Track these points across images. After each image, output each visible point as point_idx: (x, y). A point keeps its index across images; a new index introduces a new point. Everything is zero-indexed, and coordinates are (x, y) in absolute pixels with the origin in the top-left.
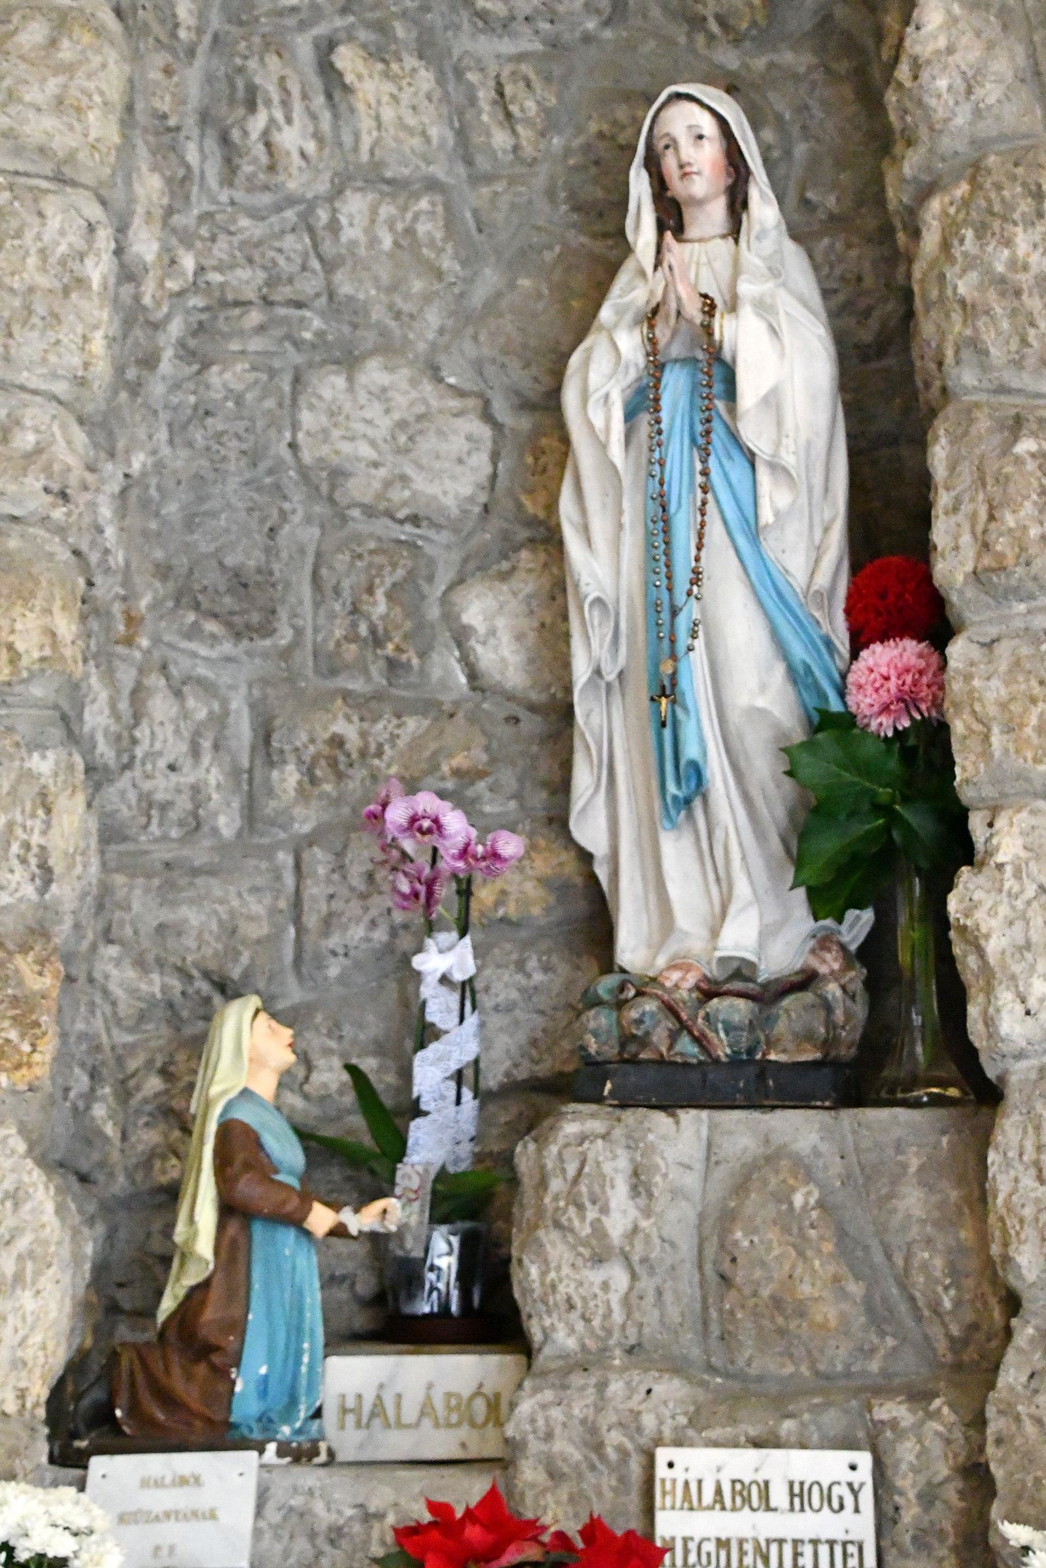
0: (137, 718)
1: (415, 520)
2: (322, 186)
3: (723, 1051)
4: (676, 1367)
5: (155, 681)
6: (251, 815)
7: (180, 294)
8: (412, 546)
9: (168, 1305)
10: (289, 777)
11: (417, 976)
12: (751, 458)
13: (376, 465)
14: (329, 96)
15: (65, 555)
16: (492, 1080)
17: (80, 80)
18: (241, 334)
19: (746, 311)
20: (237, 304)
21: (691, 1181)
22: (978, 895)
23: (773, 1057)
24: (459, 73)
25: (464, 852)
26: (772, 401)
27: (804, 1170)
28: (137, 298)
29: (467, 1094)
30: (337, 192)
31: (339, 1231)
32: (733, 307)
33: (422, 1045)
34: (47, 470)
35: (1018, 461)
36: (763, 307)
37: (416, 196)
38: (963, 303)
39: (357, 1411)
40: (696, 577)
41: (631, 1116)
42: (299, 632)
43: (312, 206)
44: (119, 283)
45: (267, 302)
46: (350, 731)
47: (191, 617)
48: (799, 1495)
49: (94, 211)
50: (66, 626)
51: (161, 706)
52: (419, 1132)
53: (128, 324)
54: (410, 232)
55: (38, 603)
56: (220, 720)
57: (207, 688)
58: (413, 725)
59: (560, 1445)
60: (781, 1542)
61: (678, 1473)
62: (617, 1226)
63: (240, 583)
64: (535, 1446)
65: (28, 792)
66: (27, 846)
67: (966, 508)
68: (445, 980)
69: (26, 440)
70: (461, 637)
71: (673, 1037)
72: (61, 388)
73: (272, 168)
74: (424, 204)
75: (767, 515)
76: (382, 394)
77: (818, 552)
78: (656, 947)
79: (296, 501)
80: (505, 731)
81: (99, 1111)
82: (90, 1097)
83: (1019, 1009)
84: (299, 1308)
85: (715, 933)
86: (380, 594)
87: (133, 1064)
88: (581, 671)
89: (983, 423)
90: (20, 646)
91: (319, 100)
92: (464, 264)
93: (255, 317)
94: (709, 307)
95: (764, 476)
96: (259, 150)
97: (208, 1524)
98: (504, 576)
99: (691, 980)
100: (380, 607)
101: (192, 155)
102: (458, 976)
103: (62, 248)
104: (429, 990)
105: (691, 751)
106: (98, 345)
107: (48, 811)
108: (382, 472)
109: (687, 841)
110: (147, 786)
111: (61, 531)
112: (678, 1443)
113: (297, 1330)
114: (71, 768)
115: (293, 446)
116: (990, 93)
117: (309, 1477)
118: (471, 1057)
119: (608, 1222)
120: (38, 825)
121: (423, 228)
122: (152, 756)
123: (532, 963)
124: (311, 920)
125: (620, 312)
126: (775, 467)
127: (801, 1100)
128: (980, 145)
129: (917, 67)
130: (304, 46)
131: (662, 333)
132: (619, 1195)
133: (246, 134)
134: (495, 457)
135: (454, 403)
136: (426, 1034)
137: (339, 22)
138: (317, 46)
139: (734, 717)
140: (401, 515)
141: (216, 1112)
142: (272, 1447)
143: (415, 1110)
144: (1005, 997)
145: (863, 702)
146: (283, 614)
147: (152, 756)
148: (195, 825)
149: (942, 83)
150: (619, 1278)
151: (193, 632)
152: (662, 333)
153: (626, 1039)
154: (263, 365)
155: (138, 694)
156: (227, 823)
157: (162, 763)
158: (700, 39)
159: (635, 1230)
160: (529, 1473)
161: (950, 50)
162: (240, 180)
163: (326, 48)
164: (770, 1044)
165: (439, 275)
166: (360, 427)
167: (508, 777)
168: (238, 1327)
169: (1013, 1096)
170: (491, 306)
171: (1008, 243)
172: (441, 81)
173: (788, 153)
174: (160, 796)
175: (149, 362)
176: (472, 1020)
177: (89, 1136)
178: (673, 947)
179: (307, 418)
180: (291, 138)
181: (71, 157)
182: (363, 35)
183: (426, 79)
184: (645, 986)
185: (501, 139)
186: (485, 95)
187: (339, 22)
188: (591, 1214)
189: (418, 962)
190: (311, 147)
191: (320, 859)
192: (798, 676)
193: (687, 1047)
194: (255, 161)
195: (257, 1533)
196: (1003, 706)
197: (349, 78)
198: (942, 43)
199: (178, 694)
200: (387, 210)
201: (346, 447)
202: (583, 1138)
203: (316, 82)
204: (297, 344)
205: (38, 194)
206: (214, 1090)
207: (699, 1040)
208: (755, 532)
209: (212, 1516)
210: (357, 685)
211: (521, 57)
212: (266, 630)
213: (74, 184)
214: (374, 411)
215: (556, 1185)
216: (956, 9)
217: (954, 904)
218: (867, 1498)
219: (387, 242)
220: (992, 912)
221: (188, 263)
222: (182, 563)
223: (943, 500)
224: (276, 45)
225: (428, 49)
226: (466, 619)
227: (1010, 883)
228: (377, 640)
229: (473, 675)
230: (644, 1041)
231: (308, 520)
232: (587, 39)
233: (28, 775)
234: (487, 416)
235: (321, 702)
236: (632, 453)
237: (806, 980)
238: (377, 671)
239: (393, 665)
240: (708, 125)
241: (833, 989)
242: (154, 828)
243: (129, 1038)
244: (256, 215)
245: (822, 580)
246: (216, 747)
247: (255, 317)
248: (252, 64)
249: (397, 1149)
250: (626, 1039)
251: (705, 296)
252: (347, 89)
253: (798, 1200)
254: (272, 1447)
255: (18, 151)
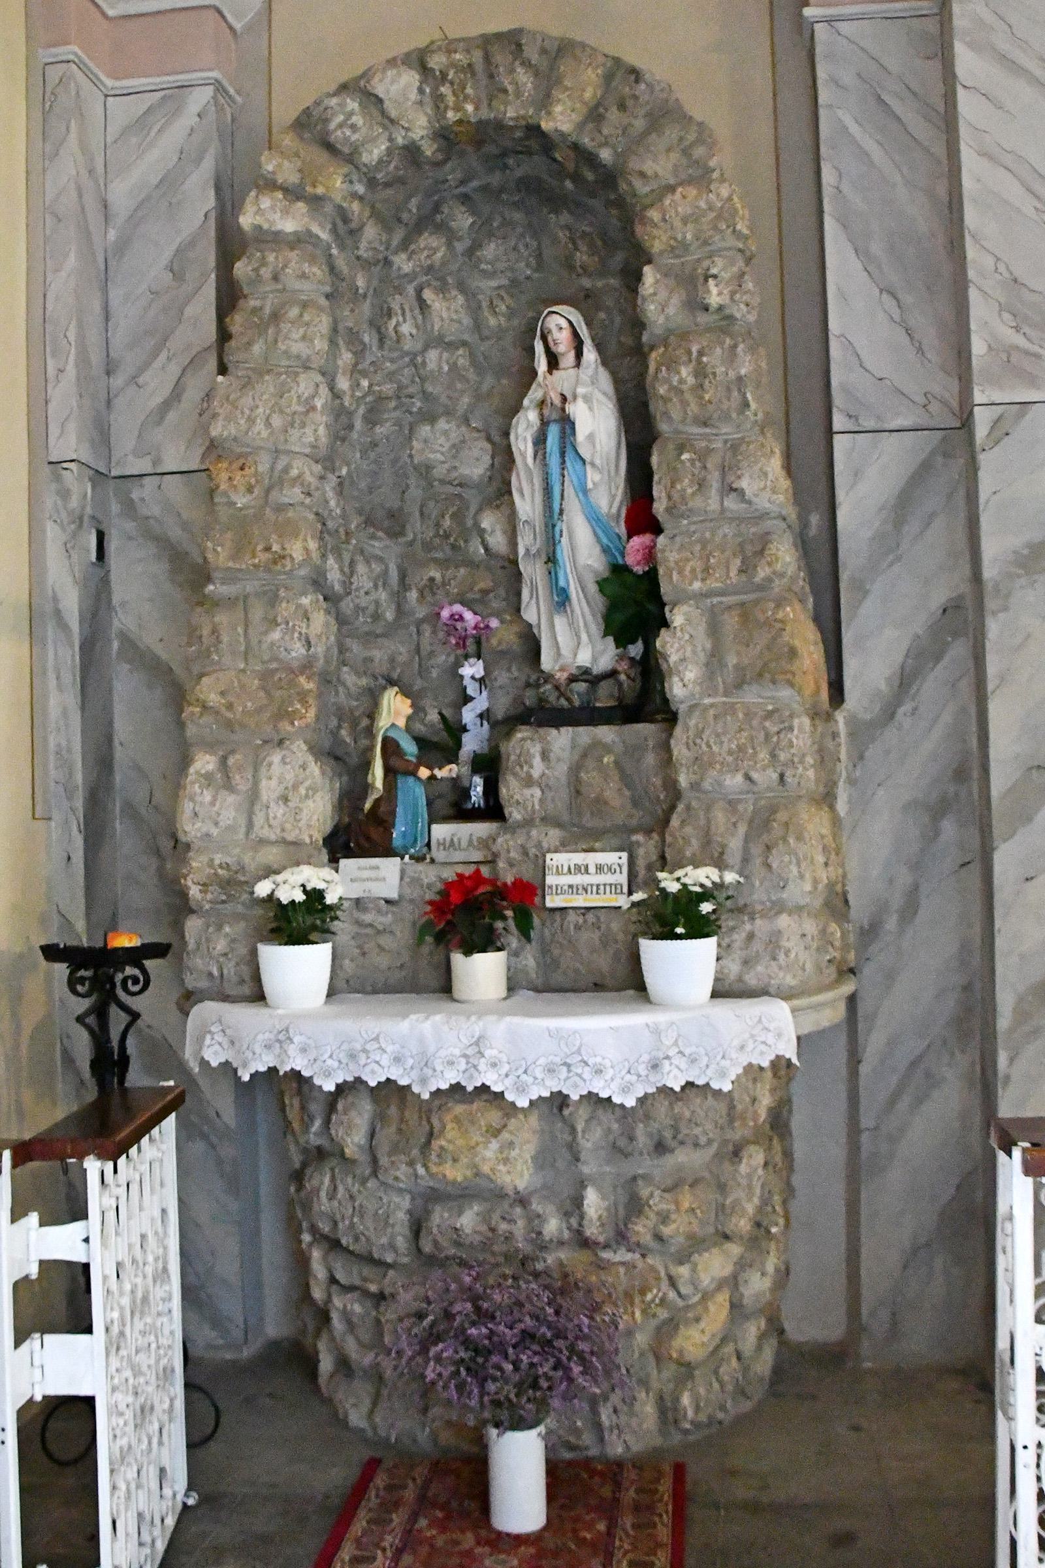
0: (352, 573)
1: (460, 485)
2: (419, 346)
3: (577, 703)
4: (559, 825)
5: (359, 558)
6: (400, 611)
7: (364, 397)
8: (459, 496)
9: (368, 806)
10: (413, 595)
11: (462, 677)
12: (584, 461)
13: (443, 462)
14: (421, 309)
15: (311, 517)
16: (500, 715)
17: (312, 329)
18: (389, 411)
19: (580, 402)
20: (387, 398)
21: (566, 755)
22: (668, 639)
23: (598, 705)
24: (474, 295)
25: (476, 627)
26: (591, 437)
27: (607, 749)
28: (342, 404)
29: (485, 723)
30: (426, 347)
31: (432, 777)
32: (575, 397)
33: (465, 704)
34: (302, 484)
35: (682, 462)
36: (587, 399)
37: (457, 348)
38: (662, 397)
39: (444, 844)
40: (561, 512)
41: (542, 731)
42: (415, 535)
43: (415, 355)
44: (333, 400)
45: (399, 398)
46: (437, 575)
47: (372, 530)
48: (600, 868)
49: (319, 378)
50: (313, 545)
51: (361, 568)
52: (466, 738)
53: (337, 416)
54: (455, 364)
55: (301, 537)
56: (386, 572)
57: (380, 559)
58: (462, 571)
59: (513, 854)
60: (592, 885)
61: (554, 863)
62: (536, 773)
63: (391, 515)
64: (503, 855)
65: (300, 612)
66: (300, 633)
67: (663, 481)
68: (473, 677)
69: (294, 472)
70: (481, 532)
71: (558, 698)
72: (307, 451)
73: (398, 341)
74: (461, 352)
75: (590, 485)
76: (446, 433)
77: (613, 497)
78: (556, 661)
79: (412, 481)
80: (499, 572)
81: (343, 732)
82: (339, 727)
83: (681, 684)
84: (416, 806)
85: (575, 655)
86: (447, 517)
87: (357, 714)
88: (521, 551)
89: (671, 446)
90: (295, 556)
91: (417, 311)
92: (479, 374)
93: (393, 404)
94: (564, 399)
95: (588, 467)
96: (393, 334)
97: (382, 883)
98: (498, 507)
99: (565, 675)
100: (447, 522)
101: (366, 339)
102: (478, 676)
103: (306, 395)
104: (467, 682)
105: (562, 583)
106: (322, 430)
107: (308, 619)
108: (446, 466)
109: (565, 620)
110: (357, 601)
111: (309, 507)
112: (556, 852)
113: (415, 815)
114: (318, 600)
115: (411, 456)
116: (671, 310)
117: (420, 867)
118: (485, 708)
119: (532, 771)
120: (304, 625)
121: (461, 361)
122: (357, 590)
123: (514, 669)
124: (424, 653)
125: (531, 402)
126: (593, 464)
127: (608, 721)
128: (670, 332)
129: (644, 299)
130: (411, 290)
131: (546, 412)
132: (537, 761)
133: (387, 329)
134: (493, 457)
135: (476, 435)
136: (467, 699)
137: (425, 278)
138: (416, 290)
139: (580, 568)
140: (456, 483)
141: (382, 732)
142: (407, 857)
143: (464, 729)
144: (676, 679)
145: (630, 560)
146: (408, 527)
147: (357, 590)
148: (376, 617)
149: (652, 307)
150: (537, 793)
151: (373, 537)
152: (546, 412)
153: (541, 700)
154: (398, 423)
155: (352, 563)
156: (390, 615)
157: (362, 592)
158: (574, 276)
159: (544, 774)
160: (501, 864)
161: (655, 294)
162: (386, 347)
163: (419, 291)
164: (596, 700)
165: (468, 381)
166: (437, 447)
167: (502, 592)
168: (393, 813)
169: (680, 717)
170: (489, 394)
171: (679, 373)
172: (467, 300)
173: (612, 322)
174: (363, 605)
175: (350, 427)
176: (485, 693)
177: (340, 742)
178: (561, 662)
179: (415, 443)
180: (406, 329)
181: (308, 359)
182: (434, 283)
183: (461, 299)
184: (548, 678)
185: (493, 322)
186: (485, 304)
187: (425, 278)
188: (525, 768)
189: (462, 671)
190: (414, 332)
191: (427, 630)
192: (605, 550)
193: (563, 702)
194: (391, 339)
195: (401, 885)
196: (676, 563)
197: (429, 302)
198: (651, 291)
199: (368, 562)
200: (445, 355)
201: (432, 456)
202: (523, 739)
203: (416, 304)
204: (411, 413)
205: (297, 374)
206: (381, 724)
207: (568, 699)
208: (585, 492)
209: (384, 879)
210: (439, 555)
211: (499, 287)
212: (402, 533)
213: (310, 368)
214: (442, 440)
215: (513, 758)
216: (658, 276)
217: (658, 643)
218: (625, 869)
219: (446, 368)
220: (672, 647)
221: (365, 383)
222: (368, 508)
223: (656, 478)
224: (399, 290)
225: (462, 287)
226: (483, 526)
227: (679, 634)
228: (447, 536)
229: (486, 549)
230: (547, 701)
231: (417, 487)
232: (528, 278)
233: (299, 606)
234: (489, 439)
235: (424, 564)
236: (538, 461)
237: (613, 674)
238: (447, 549)
239: (454, 547)
240: (564, 323)
241: (623, 677)
242: (361, 619)
243: (355, 703)
244: (392, 361)
245: (614, 510)
246: (384, 584)
247: (393, 404)
248: (389, 299)
249: (459, 745)
250: (541, 700)
251: (562, 395)
252: (429, 307)
253: (605, 760)
254: (407, 857)
255: (289, 358)
